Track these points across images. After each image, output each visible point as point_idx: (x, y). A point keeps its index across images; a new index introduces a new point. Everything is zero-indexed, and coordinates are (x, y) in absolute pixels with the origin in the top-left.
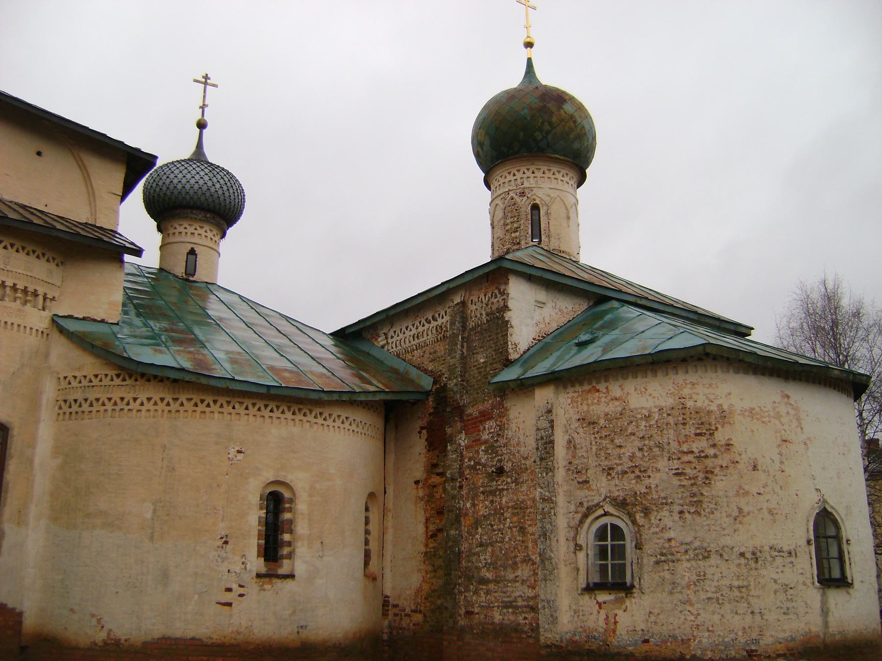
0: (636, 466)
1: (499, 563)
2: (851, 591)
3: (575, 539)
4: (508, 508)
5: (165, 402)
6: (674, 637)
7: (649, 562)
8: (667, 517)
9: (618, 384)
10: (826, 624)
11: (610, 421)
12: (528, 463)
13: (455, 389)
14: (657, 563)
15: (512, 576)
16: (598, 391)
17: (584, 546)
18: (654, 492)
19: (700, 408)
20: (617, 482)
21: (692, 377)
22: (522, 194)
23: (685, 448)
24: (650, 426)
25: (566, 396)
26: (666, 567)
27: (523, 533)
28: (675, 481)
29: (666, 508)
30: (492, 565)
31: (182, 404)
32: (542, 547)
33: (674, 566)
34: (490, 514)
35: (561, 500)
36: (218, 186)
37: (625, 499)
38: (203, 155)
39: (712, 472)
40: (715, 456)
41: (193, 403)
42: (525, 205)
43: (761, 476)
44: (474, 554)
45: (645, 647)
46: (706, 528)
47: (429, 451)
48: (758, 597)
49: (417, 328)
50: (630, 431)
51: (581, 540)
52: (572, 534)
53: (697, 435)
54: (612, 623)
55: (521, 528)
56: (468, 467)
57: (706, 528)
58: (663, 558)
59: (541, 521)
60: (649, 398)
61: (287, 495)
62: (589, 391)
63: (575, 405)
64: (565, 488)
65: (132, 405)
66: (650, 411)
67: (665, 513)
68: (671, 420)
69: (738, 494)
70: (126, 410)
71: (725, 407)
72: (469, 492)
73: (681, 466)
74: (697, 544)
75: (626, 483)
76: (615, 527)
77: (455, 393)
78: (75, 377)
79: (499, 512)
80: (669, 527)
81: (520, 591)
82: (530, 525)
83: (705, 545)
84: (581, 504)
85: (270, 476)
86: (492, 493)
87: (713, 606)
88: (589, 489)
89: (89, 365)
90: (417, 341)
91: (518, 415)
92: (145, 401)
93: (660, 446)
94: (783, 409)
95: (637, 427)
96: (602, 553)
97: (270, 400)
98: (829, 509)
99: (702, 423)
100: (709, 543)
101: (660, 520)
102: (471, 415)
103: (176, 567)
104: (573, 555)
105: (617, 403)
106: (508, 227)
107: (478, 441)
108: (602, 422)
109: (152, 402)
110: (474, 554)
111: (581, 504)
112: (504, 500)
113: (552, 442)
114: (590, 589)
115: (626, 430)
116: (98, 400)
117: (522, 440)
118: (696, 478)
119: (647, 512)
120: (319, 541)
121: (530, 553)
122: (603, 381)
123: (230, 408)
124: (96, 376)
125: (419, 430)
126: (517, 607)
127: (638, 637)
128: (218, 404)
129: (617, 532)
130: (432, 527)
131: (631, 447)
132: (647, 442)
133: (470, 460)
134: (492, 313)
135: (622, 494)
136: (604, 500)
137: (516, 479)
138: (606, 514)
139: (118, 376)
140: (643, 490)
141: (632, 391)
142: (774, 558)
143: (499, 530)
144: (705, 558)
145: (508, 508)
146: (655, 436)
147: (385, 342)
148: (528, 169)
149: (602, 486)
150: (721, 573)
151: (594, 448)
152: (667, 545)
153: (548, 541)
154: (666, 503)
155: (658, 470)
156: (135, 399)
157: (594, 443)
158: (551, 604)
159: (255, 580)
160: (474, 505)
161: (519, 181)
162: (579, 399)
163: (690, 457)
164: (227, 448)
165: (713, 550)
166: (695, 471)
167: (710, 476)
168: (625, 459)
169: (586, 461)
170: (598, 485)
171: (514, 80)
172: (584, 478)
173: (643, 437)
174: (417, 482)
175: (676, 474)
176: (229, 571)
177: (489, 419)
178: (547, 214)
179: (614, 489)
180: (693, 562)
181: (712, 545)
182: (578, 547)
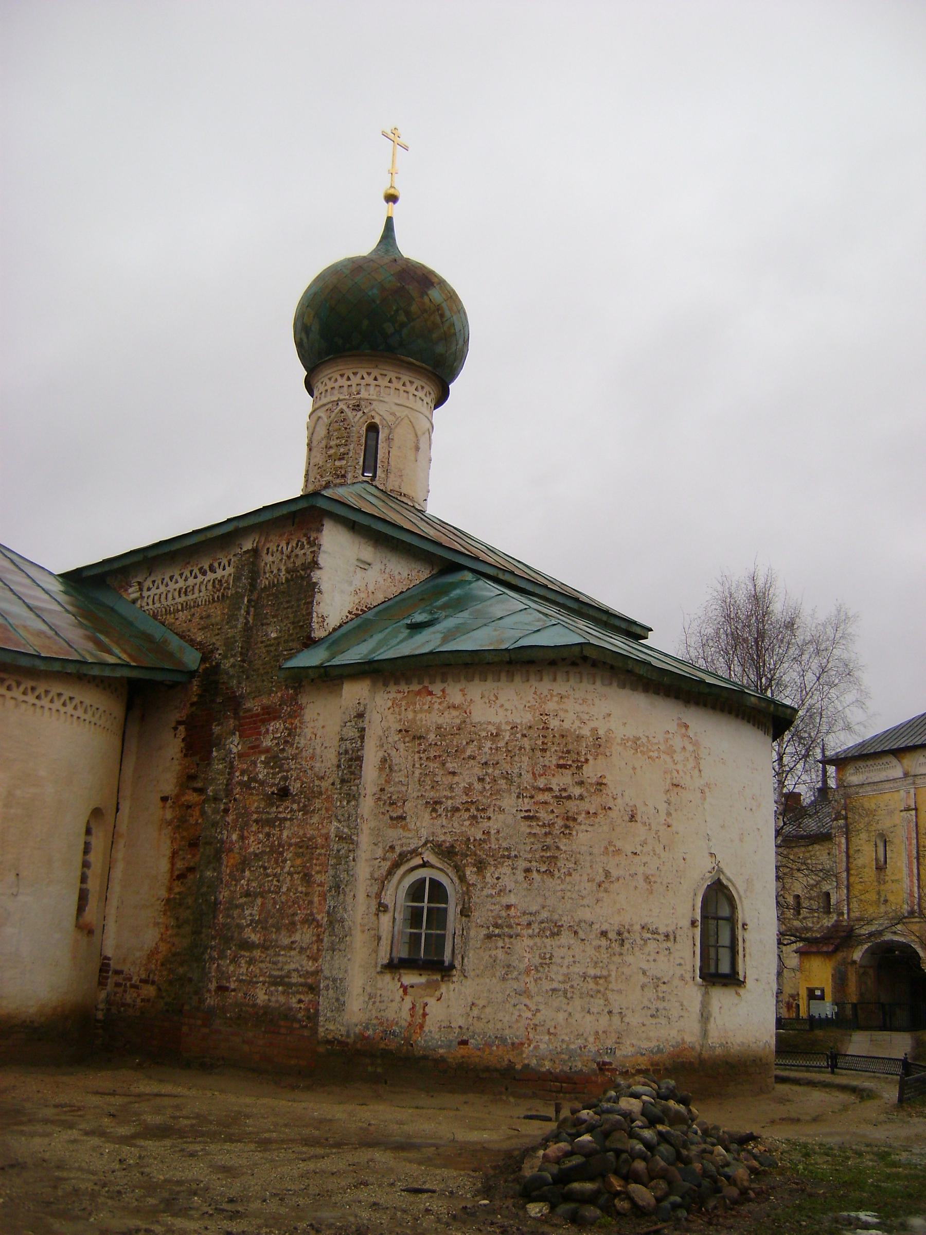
1: (270, 921)
2: (742, 991)
3: (378, 895)
4: (290, 845)
6: (503, 1040)
7: (476, 934)
8: (508, 876)
9: (459, 686)
10: (705, 1033)
11: (443, 736)
12: (325, 784)
14: (489, 937)
15: (286, 941)
17: (391, 906)
19: (569, 730)
20: (444, 823)
21: (561, 687)
22: (357, 407)
25: (386, 696)
26: (500, 944)
28: (524, 827)
30: (260, 924)
32: (332, 904)
33: (511, 943)
35: (364, 839)
37: (452, 846)
39: (575, 820)
40: (581, 798)
43: (640, 830)
44: (237, 906)
45: (463, 1050)
46: (559, 894)
47: (186, 756)
48: (620, 992)
49: (186, 580)
50: (468, 753)
51: (387, 899)
52: (376, 888)
53: (559, 766)
54: (419, 1014)
57: (559, 894)
58: (497, 931)
62: (419, 693)
63: (397, 710)
64: (373, 824)
66: (499, 728)
67: (505, 869)
68: (526, 743)
71: (601, 732)
74: (544, 915)
75: (456, 824)
79: (276, 851)
80: (508, 889)
81: (295, 963)
82: (318, 872)
83: (556, 917)
84: (392, 848)
87: (560, 1001)
88: (404, 828)
91: (316, 717)
93: (507, 777)
94: (677, 742)
96: (415, 917)
98: (725, 882)
99: (568, 752)
101: (498, 878)
104: (374, 918)
105: (455, 713)
106: (332, 452)
107: (256, 748)
108: (432, 737)
110: (237, 906)
111: (392, 848)
112: (285, 834)
113: (360, 759)
114: (394, 966)
115: (464, 751)
119: (481, 866)
121: (315, 911)
125: (173, 725)
126: (290, 985)
127: (454, 1036)
130: (180, 865)
131: (468, 775)
132: (490, 771)
133: (243, 773)
136: (425, 844)
137: (305, 806)
138: (425, 865)
140: (479, 836)
142: (645, 941)
143: (275, 875)
145: (290, 845)
148: (369, 374)
149: (423, 826)
150: (573, 956)
151: (417, 772)
152: (503, 914)
153: (342, 896)
154: (508, 856)
155: (502, 810)
157: (417, 765)
158: (337, 983)
160: (242, 838)
161: (354, 389)
162: (404, 703)
163: (547, 797)
165: (566, 925)
166: (551, 816)
167: (571, 824)
168: (458, 791)
170: (418, 824)
171: (362, 244)
172: (399, 812)
173: (486, 763)
174: (164, 799)
177: (275, 718)
179: (439, 831)
180: (537, 940)
181: (565, 918)
182: (382, 908)
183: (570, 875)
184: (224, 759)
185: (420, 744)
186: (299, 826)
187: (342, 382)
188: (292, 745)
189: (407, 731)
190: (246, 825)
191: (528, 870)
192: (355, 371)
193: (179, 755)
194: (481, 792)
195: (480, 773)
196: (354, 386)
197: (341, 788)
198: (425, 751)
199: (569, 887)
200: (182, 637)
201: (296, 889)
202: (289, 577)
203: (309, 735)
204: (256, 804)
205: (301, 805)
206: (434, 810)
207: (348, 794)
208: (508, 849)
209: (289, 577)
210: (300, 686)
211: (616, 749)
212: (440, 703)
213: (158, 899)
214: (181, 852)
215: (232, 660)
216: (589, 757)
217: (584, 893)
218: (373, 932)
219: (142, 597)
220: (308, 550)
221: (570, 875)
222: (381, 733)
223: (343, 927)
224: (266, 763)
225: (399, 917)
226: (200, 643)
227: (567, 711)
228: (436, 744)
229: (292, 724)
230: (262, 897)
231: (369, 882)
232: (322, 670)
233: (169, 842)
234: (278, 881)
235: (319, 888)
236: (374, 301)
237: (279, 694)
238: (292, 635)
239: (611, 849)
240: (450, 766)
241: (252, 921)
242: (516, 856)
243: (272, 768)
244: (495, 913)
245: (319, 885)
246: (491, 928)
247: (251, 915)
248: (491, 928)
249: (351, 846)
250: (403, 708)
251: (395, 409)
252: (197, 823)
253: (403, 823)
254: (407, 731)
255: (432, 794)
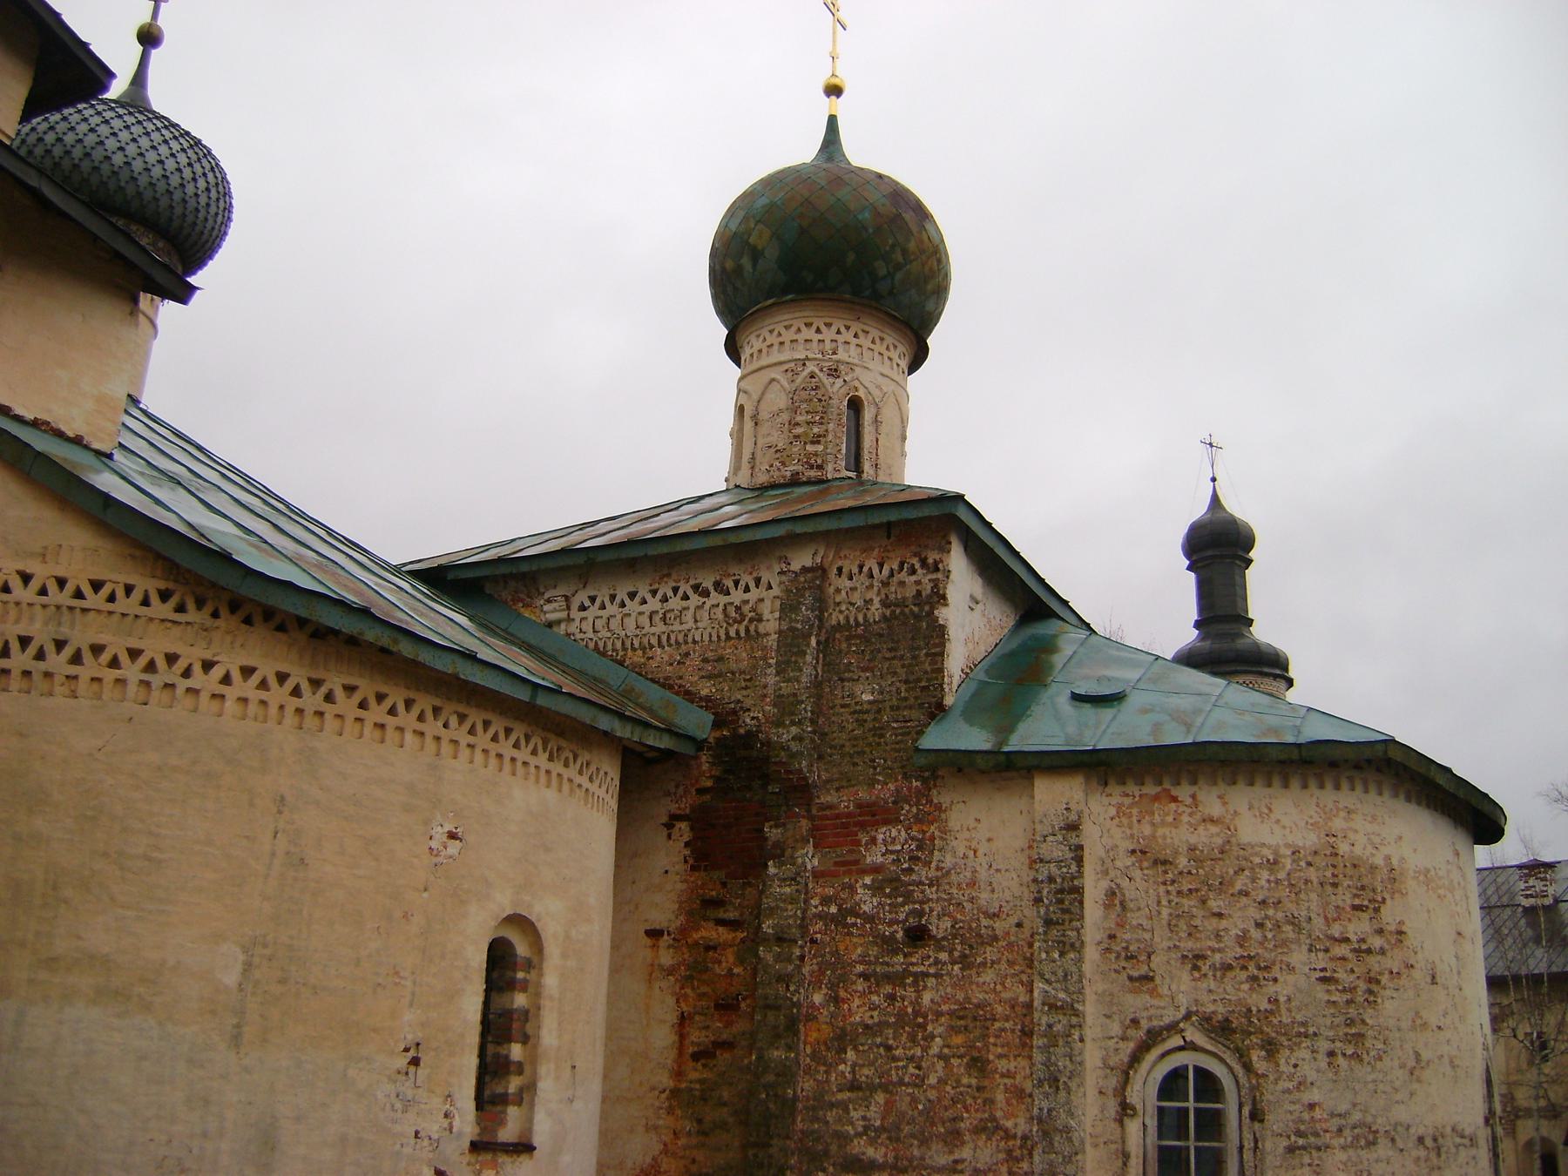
0: (1250, 958)
1: (906, 1129)
3: (1121, 1091)
4: (939, 1014)
5: (289, 685)
7: (1273, 1147)
8: (1304, 1061)
9: (1215, 791)
11: (1199, 861)
12: (1000, 926)
13: (795, 747)
14: (1291, 1150)
16: (1175, 799)
17: (1139, 1107)
18: (1283, 1011)
19: (1360, 858)
20: (1212, 986)
21: (1347, 798)
22: (834, 373)
23: (1336, 930)
24: (1277, 882)
25: (1105, 800)
26: (1307, 1160)
27: (982, 1070)
28: (1320, 992)
29: (1306, 1043)
30: (890, 1132)
31: (329, 698)
32: (1045, 1105)
33: (1320, 1158)
34: (882, 1025)
35: (1090, 1009)
36: (202, 184)
37: (1227, 1020)
38: (145, 99)
39: (1378, 982)
40: (1382, 952)
41: (357, 698)
42: (837, 390)
44: (832, 1105)
46: (1371, 1086)
47: (693, 868)
49: (665, 599)
50: (1238, 886)
51: (1133, 1097)
52: (1113, 1082)
53: (1356, 908)
55: (974, 1060)
56: (820, 916)
57: (1371, 1086)
58: (1301, 1142)
59: (1045, 1049)
60: (1275, 827)
61: (522, 949)
62: (1156, 798)
63: (1125, 821)
64: (1100, 987)
65: (198, 679)
66: (1276, 853)
67: (1303, 1053)
68: (1312, 874)
69: (1413, 1028)
70: (180, 691)
71: (1395, 862)
72: (822, 972)
73: (1330, 966)
74: (1356, 1116)
75: (1229, 989)
76: (1203, 1075)
77: (793, 756)
78: (26, 578)
79: (914, 1024)
80: (1305, 1082)
82: (1000, 1056)
83: (1369, 1119)
84: (1135, 1022)
85: (504, 902)
86: (897, 979)
88: (1153, 992)
89: (78, 552)
90: (660, 628)
91: (972, 824)
92: (236, 675)
93: (1293, 921)
95: (1254, 880)
96: (1170, 1123)
97: (517, 718)
99: (1363, 888)
100: (1374, 1117)
101: (1295, 1066)
102: (831, 807)
103: (298, 1119)
104: (1115, 1125)
105: (1214, 829)
106: (799, 430)
107: (854, 866)
108: (1182, 862)
109: (255, 679)
110: (832, 1105)
111: (1135, 1022)
112: (927, 997)
113: (1079, 891)
115: (1232, 884)
116: (97, 650)
117: (983, 875)
118: (1352, 990)
119: (1271, 1049)
120: (569, 1064)
121: (999, 1114)
122: (1184, 782)
123: (440, 724)
124: (97, 586)
125: (665, 819)
128: (415, 711)
129: (1208, 1084)
130: (696, 1036)
131: (1241, 918)
132: (1271, 912)
133: (826, 901)
134: (902, 603)
135: (1221, 1009)
136: (1187, 1017)
137: (964, 956)
138: (1189, 1046)
139: (165, 596)
140: (1264, 1005)
141: (1243, 808)
143: (911, 1059)
144: (1371, 1144)
145: (939, 1014)
146: (1285, 901)
147: (563, 615)
148: (848, 328)
149: (1181, 991)
151: (1165, 912)
152: (1306, 1116)
153: (1063, 1094)
155: (1291, 969)
156: (208, 666)
157: (1164, 902)
159: (468, 1157)
161: (828, 346)
162: (1135, 811)
163: (1341, 950)
164: (427, 822)
165: (1382, 1130)
166: (1352, 977)
167: (1375, 988)
168: (1228, 941)
169: (1147, 936)
170: (1174, 987)
171: (803, 150)
172: (1143, 970)
173: (1263, 902)
174: (654, 934)
175: (1323, 980)
176: (417, 1133)
177: (886, 822)
178: (876, 421)
179: (1205, 998)
180: (1351, 1152)
181: (1379, 1121)
182: (1126, 1110)
183: (1380, 1059)
184: (794, 879)
185: (1166, 872)
186: (954, 986)
187: (808, 333)
188: (928, 864)
189: (1143, 852)
190: (843, 979)
191: (1331, 1054)
192: (828, 320)
193: (681, 867)
194: (1261, 944)
195: (1258, 916)
196: (827, 342)
197: (1045, 933)
198: (1173, 882)
199: (1381, 1076)
200: (666, 685)
201: (958, 1081)
202: (888, 613)
203: (961, 851)
204: (859, 951)
205: (956, 954)
206: (1196, 968)
207: (1059, 942)
208: (1304, 1024)
209: (888, 613)
210: (935, 777)
211: (1411, 884)
212: (1191, 815)
213: (653, 1089)
214: (697, 1018)
215: (794, 730)
216: (1387, 896)
217: (1397, 1084)
218: (1113, 1147)
219: (569, 620)
220: (925, 578)
221: (1380, 1059)
222: (1102, 853)
223: (1070, 1140)
224: (876, 889)
225: (1152, 1123)
226: (708, 699)
227: (1356, 831)
228: (1189, 873)
229: (924, 832)
230: (886, 1091)
231: (1099, 1072)
232: (1002, 758)
233: (671, 1001)
234: (919, 1068)
235: (1006, 1080)
236: (866, 229)
237: (891, 786)
238: (906, 699)
239: (1419, 1022)
240: (1214, 904)
241: (866, 1128)
242: (1315, 1034)
243: (889, 896)
244: (1297, 1114)
245: (1003, 1076)
246: (1293, 1138)
247: (864, 1118)
248: (1293, 1138)
249: (1074, 1020)
250: (1134, 819)
251: (880, 378)
252: (730, 973)
253: (1151, 985)
254: (1143, 852)
255: (1190, 944)
